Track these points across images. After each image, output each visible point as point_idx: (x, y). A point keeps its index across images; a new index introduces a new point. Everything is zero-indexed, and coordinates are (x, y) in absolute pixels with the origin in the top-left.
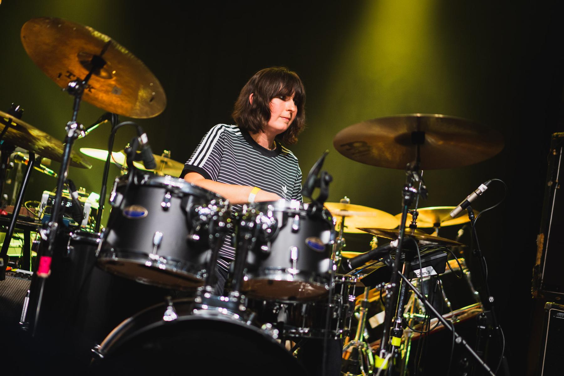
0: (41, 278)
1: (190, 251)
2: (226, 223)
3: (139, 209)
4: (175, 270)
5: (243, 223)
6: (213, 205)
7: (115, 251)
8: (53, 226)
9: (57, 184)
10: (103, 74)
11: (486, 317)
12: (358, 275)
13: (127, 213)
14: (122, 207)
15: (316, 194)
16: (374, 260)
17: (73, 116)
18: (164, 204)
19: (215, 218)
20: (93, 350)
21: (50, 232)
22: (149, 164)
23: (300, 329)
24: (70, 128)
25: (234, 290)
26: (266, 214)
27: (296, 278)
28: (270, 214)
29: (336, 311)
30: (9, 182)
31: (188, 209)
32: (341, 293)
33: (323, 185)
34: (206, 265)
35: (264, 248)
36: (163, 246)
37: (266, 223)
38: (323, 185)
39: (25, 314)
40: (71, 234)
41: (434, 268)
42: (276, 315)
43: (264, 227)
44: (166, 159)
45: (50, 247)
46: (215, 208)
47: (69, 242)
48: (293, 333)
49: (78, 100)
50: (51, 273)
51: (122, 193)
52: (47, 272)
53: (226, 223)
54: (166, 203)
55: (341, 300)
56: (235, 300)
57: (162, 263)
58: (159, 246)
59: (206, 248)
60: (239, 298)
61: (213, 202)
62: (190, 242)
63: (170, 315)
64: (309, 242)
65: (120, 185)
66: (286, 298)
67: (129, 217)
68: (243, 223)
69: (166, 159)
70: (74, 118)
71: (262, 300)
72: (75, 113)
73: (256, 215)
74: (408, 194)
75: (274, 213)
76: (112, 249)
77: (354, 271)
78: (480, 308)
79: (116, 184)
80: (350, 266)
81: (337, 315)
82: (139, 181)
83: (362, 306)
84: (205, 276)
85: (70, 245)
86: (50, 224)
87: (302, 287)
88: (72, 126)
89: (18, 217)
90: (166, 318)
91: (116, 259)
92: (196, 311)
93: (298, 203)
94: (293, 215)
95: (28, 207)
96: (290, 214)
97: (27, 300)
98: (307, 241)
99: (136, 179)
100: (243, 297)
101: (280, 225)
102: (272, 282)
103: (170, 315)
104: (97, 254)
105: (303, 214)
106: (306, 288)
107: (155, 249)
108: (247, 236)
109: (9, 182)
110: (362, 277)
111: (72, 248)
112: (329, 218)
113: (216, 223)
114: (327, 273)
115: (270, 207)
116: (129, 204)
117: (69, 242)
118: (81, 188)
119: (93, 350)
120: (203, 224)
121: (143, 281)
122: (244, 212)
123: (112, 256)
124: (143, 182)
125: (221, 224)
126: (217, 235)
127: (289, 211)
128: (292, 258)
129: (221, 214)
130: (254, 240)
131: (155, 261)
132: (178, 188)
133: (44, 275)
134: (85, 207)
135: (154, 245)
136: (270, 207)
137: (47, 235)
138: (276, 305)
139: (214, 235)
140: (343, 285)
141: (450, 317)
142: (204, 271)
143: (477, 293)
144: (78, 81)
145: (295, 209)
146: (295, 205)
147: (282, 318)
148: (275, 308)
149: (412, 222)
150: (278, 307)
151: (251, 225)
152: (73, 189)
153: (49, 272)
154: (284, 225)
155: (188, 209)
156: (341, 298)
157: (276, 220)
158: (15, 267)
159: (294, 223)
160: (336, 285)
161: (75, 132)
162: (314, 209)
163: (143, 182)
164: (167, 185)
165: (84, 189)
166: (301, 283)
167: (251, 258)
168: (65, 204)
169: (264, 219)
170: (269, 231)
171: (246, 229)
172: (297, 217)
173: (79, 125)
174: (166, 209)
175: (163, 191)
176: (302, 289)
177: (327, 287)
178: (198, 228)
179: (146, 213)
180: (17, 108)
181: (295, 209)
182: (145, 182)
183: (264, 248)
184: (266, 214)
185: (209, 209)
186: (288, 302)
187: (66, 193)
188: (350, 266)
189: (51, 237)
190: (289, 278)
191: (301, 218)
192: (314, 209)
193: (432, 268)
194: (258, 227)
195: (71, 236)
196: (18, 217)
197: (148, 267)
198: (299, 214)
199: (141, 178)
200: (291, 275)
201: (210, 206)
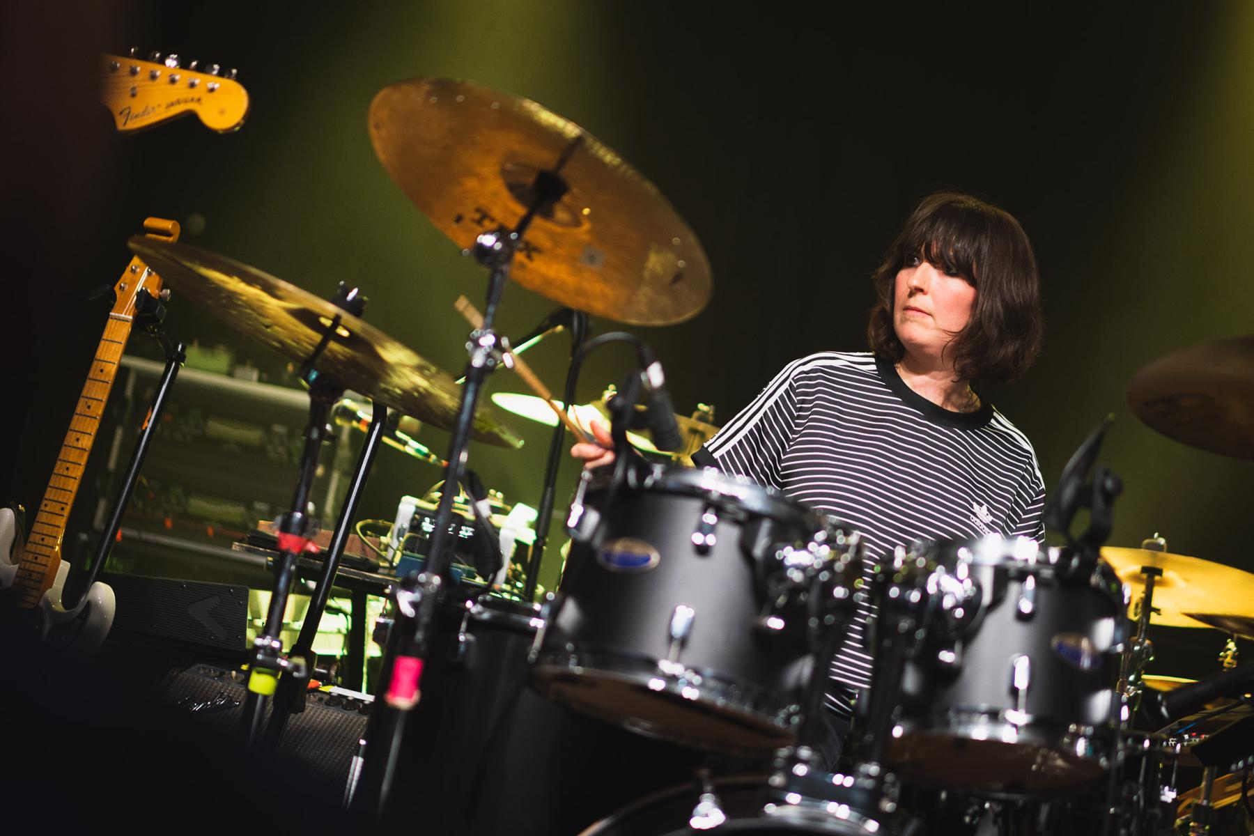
0: (395, 711)
1: (757, 659)
2: (853, 590)
3: (638, 549)
4: (720, 702)
5: (894, 592)
8: (429, 583)
12: (1186, 737)
13: (608, 556)
15: (1081, 525)
18: (698, 539)
19: (824, 576)
21: (423, 596)
24: (477, 345)
25: (868, 760)
26: (952, 570)
28: (962, 570)
31: (758, 551)
32: (1141, 779)
33: (1099, 501)
34: (798, 694)
35: (947, 657)
36: (695, 642)
38: (1099, 501)
43: (948, 603)
44: (701, 426)
45: (419, 636)
47: (464, 626)
51: (597, 508)
52: (410, 696)
54: (705, 535)
55: (1139, 797)
56: (868, 783)
58: (683, 642)
60: (879, 779)
61: (820, 536)
62: (762, 636)
63: (708, 815)
64: (1060, 646)
65: (593, 487)
66: (999, 785)
67: (614, 566)
68: (894, 592)
69: (701, 426)
73: (928, 572)
75: (973, 568)
82: (641, 478)
85: (468, 631)
86: (422, 577)
87: (1039, 760)
88: (482, 341)
90: (697, 822)
92: (771, 809)
94: (1021, 576)
95: (365, 534)
96: (1012, 573)
98: (1055, 642)
99: (632, 476)
100: (890, 778)
101: (987, 598)
105: (1047, 573)
106: (1050, 762)
107: (674, 649)
108: (904, 625)
113: (828, 588)
115: (963, 553)
117: (464, 626)
120: (796, 589)
121: (641, 728)
122: (898, 564)
124: (649, 481)
125: (839, 592)
126: (830, 619)
127: (1010, 564)
128: (1017, 684)
129: (839, 566)
130: (920, 634)
131: (672, 679)
135: (671, 638)
136: (963, 553)
137: (414, 605)
139: (821, 617)
140: (1144, 761)
144: (502, 233)
145: (1026, 560)
146: (1026, 550)
148: (971, 811)
154: (998, 600)
155: (758, 551)
156: (1140, 792)
157: (979, 587)
158: (327, 680)
159: (1023, 597)
162: (1075, 562)
163: (649, 481)
164: (708, 491)
166: (1036, 750)
167: (910, 681)
168: (457, 530)
169: (948, 583)
171: (902, 603)
172: (1030, 582)
174: (703, 550)
175: (696, 505)
176: (1039, 766)
177: (1103, 761)
179: (655, 558)
181: (1026, 560)
182: (655, 483)
183: (947, 657)
184: (952, 570)
189: (422, 610)
190: (1008, 735)
191: (1040, 582)
192: (1075, 562)
195: (468, 610)
197: (654, 693)
198: (1036, 574)
199: (644, 470)
200: (1013, 728)
201: (812, 546)
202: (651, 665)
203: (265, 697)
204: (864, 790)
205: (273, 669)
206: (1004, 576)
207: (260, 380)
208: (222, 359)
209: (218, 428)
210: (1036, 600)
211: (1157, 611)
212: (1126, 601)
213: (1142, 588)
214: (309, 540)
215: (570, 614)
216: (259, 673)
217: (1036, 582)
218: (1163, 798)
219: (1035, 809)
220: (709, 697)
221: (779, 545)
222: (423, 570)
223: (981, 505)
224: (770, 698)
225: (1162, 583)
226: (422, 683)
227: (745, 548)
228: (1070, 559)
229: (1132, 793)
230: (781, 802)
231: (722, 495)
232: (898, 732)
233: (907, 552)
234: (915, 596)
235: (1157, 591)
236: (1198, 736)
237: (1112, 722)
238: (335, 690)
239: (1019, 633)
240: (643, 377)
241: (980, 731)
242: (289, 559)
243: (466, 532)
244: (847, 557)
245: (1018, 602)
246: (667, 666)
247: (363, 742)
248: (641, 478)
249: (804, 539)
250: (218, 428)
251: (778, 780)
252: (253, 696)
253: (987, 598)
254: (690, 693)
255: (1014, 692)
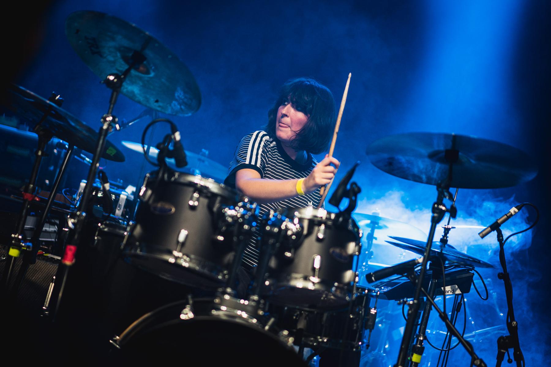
0: (65, 266)
1: (210, 252)
2: (251, 226)
3: (167, 206)
4: (197, 268)
5: (268, 228)
6: (240, 207)
7: (140, 245)
8: (81, 215)
9: (91, 174)
10: (141, 68)
11: (507, 341)
12: (383, 288)
13: (155, 208)
14: (151, 202)
15: (345, 204)
16: (398, 274)
17: (109, 108)
18: (191, 203)
19: (241, 220)
20: (111, 341)
22: (182, 162)
23: (319, 337)
25: (254, 294)
26: (292, 220)
27: (317, 287)
28: (296, 221)
29: (357, 323)
30: (52, 168)
31: (215, 209)
32: (363, 305)
34: (228, 267)
35: (288, 254)
36: (188, 244)
37: (292, 230)
39: (48, 302)
40: (99, 225)
41: (459, 287)
42: (296, 321)
43: (289, 233)
44: (203, 158)
45: (76, 237)
46: (242, 210)
47: (97, 233)
48: (311, 341)
49: (115, 94)
50: (76, 262)
51: (151, 189)
53: (251, 226)
54: (194, 202)
55: (362, 312)
56: (253, 304)
57: (185, 261)
58: (183, 244)
59: (230, 250)
60: (258, 302)
61: (241, 204)
63: (187, 314)
64: (333, 252)
66: (307, 305)
68: (268, 228)
69: (203, 158)
70: (110, 111)
71: (282, 304)
72: (112, 106)
73: (282, 221)
74: (437, 211)
75: (301, 220)
76: (137, 243)
77: (378, 282)
78: (504, 330)
79: (146, 179)
80: (373, 278)
81: (357, 326)
83: (386, 319)
84: (227, 277)
86: (78, 213)
87: (324, 296)
89: (53, 203)
90: (183, 317)
91: (141, 253)
92: (214, 312)
93: (325, 212)
94: (319, 223)
95: (66, 194)
96: (316, 223)
97: (52, 285)
98: (331, 250)
99: (166, 176)
100: (262, 301)
101: (305, 232)
102: (294, 288)
103: (187, 314)
104: (122, 247)
105: (330, 223)
106: (329, 297)
108: (271, 241)
109: (52, 168)
110: (386, 290)
111: (100, 238)
112: (356, 229)
113: (242, 224)
114: (349, 284)
116: (156, 201)
117: (97, 233)
118: (119, 180)
119: (111, 341)
120: (229, 225)
121: (166, 277)
122: (271, 216)
123: (136, 250)
124: (173, 179)
125: (246, 227)
126: (241, 237)
127: (316, 219)
128: (315, 266)
129: (246, 217)
130: (278, 245)
131: (177, 258)
132: (206, 188)
133: (68, 263)
134: (120, 198)
135: (178, 242)
136: (296, 213)
137: (73, 223)
138: (296, 312)
139: (238, 237)
140: (365, 298)
141: (473, 336)
142: (225, 272)
143: (502, 314)
144: (117, 76)
146: (322, 213)
147: (301, 325)
148: (296, 314)
149: (444, 237)
150: (298, 313)
151: (276, 230)
152: (104, 180)
153: (74, 261)
154: (310, 232)
155: (215, 209)
156: (363, 310)
157: (302, 227)
158: (47, 251)
160: (358, 297)
161: (109, 125)
162: (341, 219)
163: (173, 179)
164: (197, 184)
165: (122, 181)
166: (323, 292)
167: (273, 263)
168: (97, 194)
169: (290, 225)
170: (294, 237)
171: (271, 233)
172: (323, 227)
173: (114, 118)
174: (193, 208)
175: (191, 189)
176: (324, 298)
177: (347, 298)
178: (224, 228)
179: (173, 210)
180: (57, 98)
182: (175, 179)
184: (292, 220)
185: (236, 210)
186: (307, 309)
187: (98, 184)
188: (373, 278)
189: (78, 226)
190: (310, 286)
191: (327, 227)
192: (341, 219)
193: (457, 287)
194: (282, 233)
195: (99, 227)
196: (53, 203)
197: (171, 263)
198: (325, 223)
199: (172, 174)
200: (312, 284)
201: (237, 208)
202: (170, 253)
203: (15, 258)
204: (252, 306)
205: (18, 247)
206: (314, 223)
207: (29, 131)
208: (15, 121)
209: (11, 149)
210: (325, 233)
211: (376, 239)
212: (361, 235)
213: (370, 229)
214: (36, 196)
215: (138, 230)
216: (13, 248)
217: (325, 226)
218: (371, 313)
219: (322, 315)
220: (192, 265)
221: (224, 207)
222: (79, 211)
223: (310, 202)
224: (218, 266)
225: (380, 228)
226: (76, 255)
227: (210, 207)
228: (339, 218)
229: (360, 310)
230: (219, 309)
231: (202, 186)
232: (267, 283)
233: (275, 212)
234: (276, 230)
235: (376, 231)
236: (387, 287)
237: (352, 283)
238: (50, 255)
239: (317, 246)
240: (173, 137)
241: (299, 284)
242: (27, 202)
243: (100, 195)
244: (249, 213)
245: (317, 234)
246: (176, 253)
247: (54, 277)
248: (170, 177)
249: (233, 204)
250: (11, 149)
251: (217, 301)
252: (11, 257)
253: (305, 232)
254: (186, 265)
255: (314, 269)
